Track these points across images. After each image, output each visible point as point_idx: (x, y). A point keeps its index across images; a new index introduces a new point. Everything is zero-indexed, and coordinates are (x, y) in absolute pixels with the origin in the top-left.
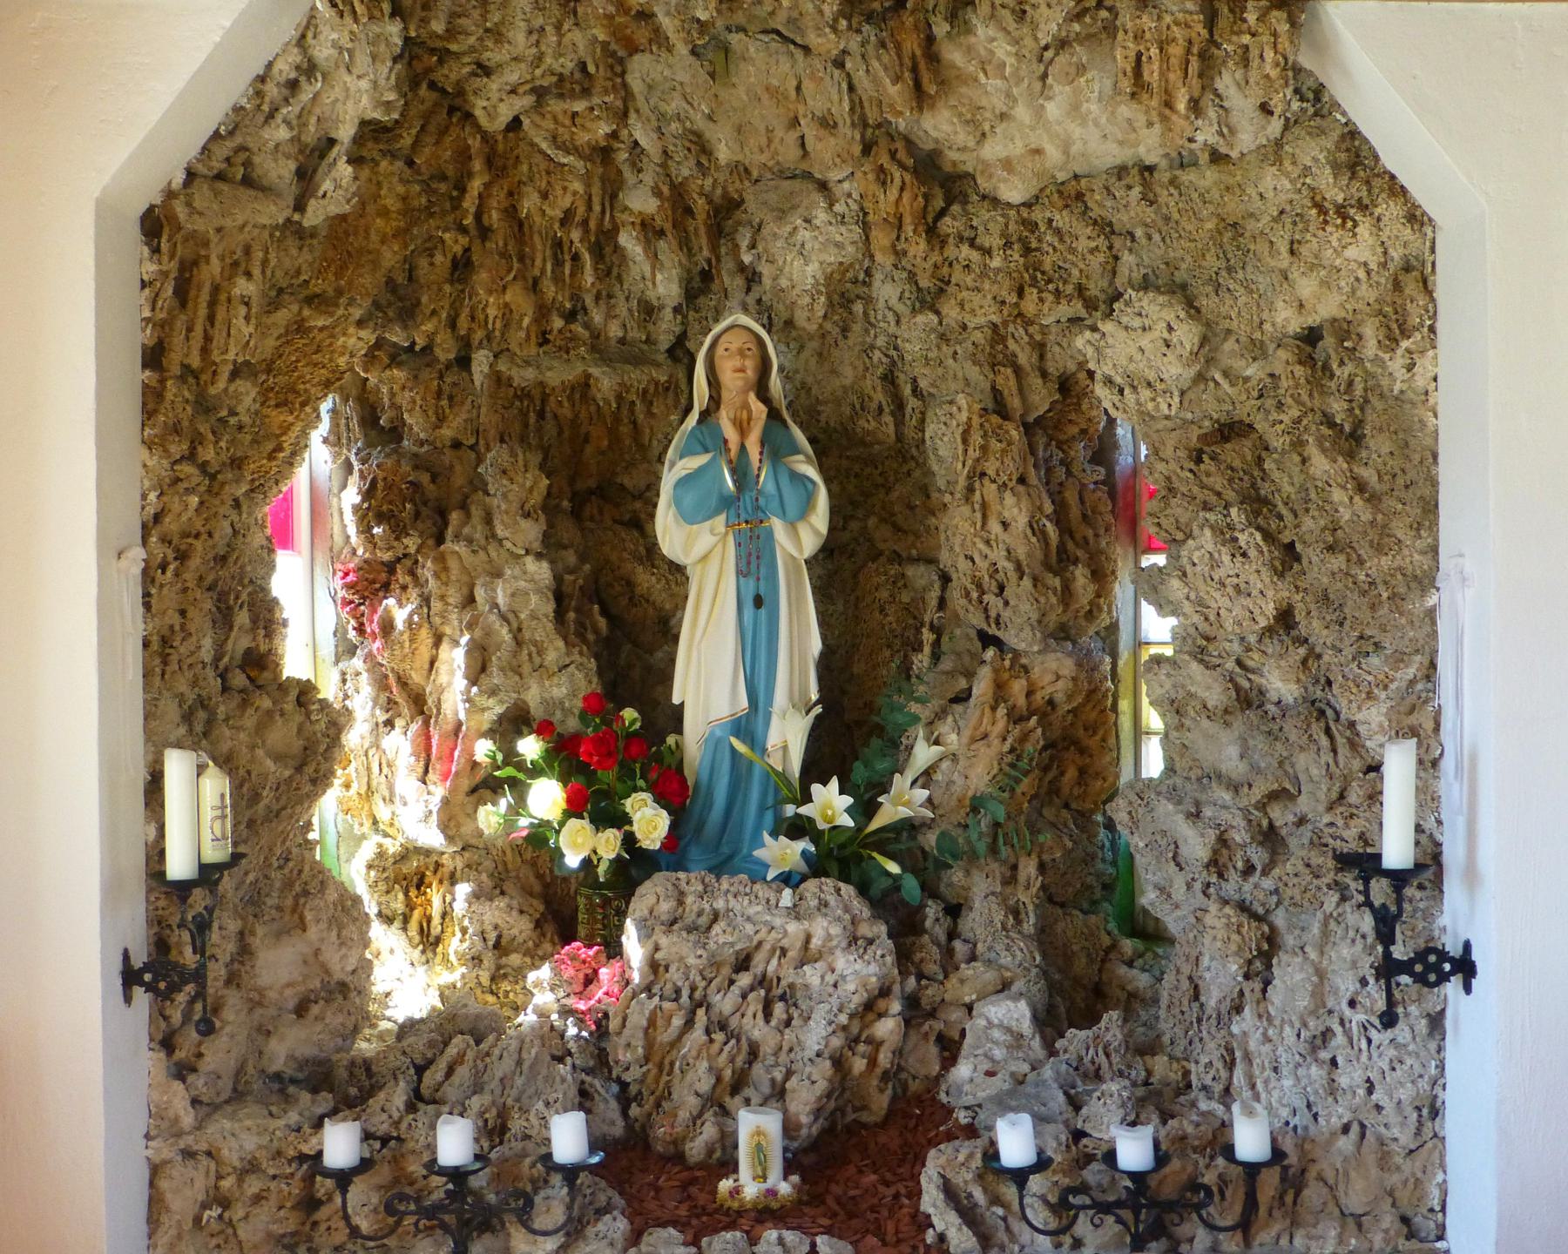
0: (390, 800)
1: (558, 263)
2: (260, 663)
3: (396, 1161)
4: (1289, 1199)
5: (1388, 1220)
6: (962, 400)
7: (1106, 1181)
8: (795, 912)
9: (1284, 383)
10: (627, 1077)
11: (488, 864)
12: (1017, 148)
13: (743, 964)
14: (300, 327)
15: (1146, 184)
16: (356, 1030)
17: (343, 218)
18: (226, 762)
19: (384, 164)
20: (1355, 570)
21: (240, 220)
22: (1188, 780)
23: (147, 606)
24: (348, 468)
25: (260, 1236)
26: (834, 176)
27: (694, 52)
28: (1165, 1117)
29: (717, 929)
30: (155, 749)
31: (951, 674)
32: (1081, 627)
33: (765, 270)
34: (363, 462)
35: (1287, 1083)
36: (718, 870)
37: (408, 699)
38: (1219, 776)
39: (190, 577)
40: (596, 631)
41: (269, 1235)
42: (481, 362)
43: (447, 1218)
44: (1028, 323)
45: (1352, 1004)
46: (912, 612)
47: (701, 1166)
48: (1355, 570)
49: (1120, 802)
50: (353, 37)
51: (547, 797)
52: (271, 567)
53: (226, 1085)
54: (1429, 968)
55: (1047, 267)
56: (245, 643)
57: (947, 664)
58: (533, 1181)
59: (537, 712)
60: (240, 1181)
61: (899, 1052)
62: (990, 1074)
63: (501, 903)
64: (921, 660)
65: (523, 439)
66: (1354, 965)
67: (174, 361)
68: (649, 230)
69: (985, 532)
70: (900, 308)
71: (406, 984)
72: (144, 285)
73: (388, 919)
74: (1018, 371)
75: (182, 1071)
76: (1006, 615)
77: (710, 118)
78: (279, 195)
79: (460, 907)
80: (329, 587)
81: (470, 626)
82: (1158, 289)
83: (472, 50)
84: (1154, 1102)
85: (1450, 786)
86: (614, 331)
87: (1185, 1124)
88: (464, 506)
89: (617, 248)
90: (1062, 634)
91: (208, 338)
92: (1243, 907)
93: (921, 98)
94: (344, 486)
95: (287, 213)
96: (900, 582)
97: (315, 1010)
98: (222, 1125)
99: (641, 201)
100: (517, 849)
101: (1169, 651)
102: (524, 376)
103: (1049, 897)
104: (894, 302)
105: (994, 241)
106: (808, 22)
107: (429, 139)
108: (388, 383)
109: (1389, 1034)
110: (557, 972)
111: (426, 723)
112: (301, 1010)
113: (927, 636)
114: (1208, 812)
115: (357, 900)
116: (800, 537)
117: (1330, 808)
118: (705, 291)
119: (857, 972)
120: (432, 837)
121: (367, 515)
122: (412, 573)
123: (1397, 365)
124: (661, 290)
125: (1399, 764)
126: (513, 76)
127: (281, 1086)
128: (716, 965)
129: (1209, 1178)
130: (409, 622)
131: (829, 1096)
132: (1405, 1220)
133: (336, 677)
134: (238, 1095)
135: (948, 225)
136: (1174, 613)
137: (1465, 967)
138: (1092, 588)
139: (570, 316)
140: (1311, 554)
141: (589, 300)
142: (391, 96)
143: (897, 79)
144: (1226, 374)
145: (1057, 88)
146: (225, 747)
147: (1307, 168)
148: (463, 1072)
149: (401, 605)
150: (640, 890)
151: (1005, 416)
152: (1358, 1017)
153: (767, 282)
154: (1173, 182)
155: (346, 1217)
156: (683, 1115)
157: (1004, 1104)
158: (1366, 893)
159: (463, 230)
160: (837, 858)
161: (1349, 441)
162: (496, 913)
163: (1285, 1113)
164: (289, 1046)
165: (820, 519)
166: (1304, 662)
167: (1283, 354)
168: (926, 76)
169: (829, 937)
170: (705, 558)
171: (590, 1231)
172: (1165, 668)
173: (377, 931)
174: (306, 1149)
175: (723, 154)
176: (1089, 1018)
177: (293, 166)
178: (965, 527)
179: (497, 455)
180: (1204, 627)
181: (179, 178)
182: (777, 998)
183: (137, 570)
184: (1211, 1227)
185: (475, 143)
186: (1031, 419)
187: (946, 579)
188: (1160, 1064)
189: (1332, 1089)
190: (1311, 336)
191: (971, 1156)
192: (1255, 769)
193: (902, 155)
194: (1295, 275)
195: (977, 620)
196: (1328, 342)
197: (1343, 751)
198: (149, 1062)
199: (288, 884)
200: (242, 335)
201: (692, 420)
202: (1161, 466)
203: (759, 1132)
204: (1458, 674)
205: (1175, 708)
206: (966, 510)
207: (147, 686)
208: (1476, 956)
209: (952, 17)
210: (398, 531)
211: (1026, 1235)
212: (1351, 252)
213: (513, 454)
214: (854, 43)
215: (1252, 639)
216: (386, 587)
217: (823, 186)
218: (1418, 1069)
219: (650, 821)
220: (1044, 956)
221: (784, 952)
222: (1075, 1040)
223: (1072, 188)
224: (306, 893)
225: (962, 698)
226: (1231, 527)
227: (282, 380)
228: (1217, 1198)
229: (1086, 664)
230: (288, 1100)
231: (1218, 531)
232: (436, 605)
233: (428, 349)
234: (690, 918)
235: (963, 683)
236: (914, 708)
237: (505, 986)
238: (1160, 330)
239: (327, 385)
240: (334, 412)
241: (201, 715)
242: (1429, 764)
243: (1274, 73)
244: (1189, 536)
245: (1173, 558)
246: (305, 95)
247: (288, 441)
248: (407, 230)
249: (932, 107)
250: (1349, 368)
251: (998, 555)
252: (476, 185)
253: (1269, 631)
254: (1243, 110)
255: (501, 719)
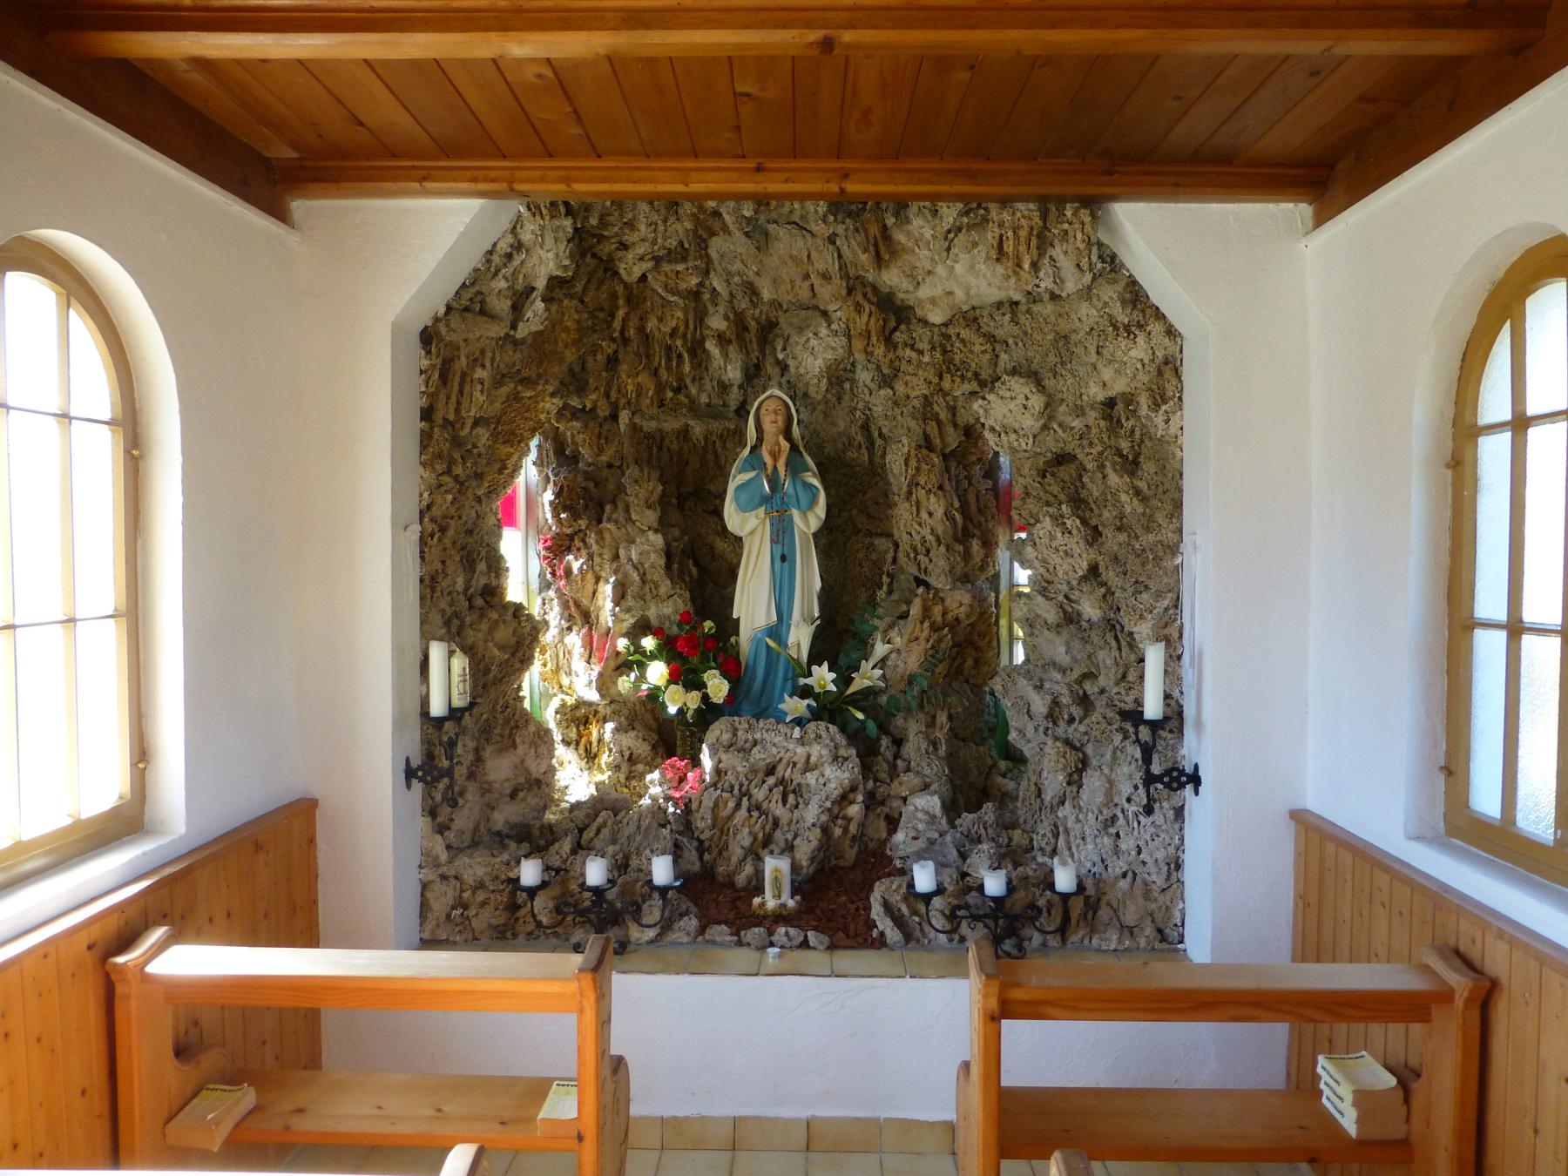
0: (569, 673)
1: (669, 359)
2: (492, 593)
3: (564, 883)
4: (1090, 915)
5: (1149, 930)
6: (905, 440)
7: (979, 902)
8: (802, 741)
9: (1094, 431)
10: (703, 837)
11: (625, 711)
12: (938, 292)
13: (771, 771)
14: (516, 397)
15: (1014, 313)
16: (545, 807)
17: (540, 333)
18: (469, 651)
19: (566, 302)
20: (1133, 542)
21: (478, 334)
22: (1037, 669)
23: (422, 558)
24: (547, 479)
25: (485, 925)
26: (831, 308)
27: (747, 234)
28: (1016, 865)
29: (755, 750)
30: (426, 637)
31: (898, 602)
32: (976, 574)
33: (791, 363)
34: (556, 475)
35: (1090, 847)
36: (758, 717)
37: (580, 614)
38: (1054, 664)
39: (447, 542)
40: (691, 576)
41: (490, 925)
42: (624, 417)
43: (592, 916)
44: (946, 394)
45: (1129, 800)
46: (878, 565)
47: (744, 889)
48: (1133, 542)
49: (997, 679)
50: (542, 228)
51: (657, 672)
52: (499, 536)
53: (467, 838)
54: (1172, 780)
55: (957, 361)
56: (483, 580)
57: (895, 596)
58: (643, 896)
59: (654, 622)
60: (474, 893)
61: (862, 825)
62: (915, 838)
63: (632, 734)
64: (882, 594)
65: (649, 462)
66: (1130, 777)
67: (438, 417)
68: (722, 340)
69: (919, 518)
70: (872, 386)
71: (576, 781)
72: (421, 372)
73: (566, 743)
74: (939, 423)
75: (441, 829)
76: (930, 567)
77: (757, 274)
78: (501, 320)
79: (608, 736)
80: (536, 548)
81: (616, 572)
82: (1020, 375)
83: (617, 234)
84: (1008, 857)
85: (1187, 670)
86: (704, 399)
87: (1029, 870)
88: (614, 502)
89: (705, 350)
90: (965, 579)
91: (459, 403)
92: (1067, 742)
93: (879, 262)
94: (545, 490)
95: (506, 330)
96: (871, 547)
97: (521, 795)
98: (464, 860)
99: (717, 322)
100: (643, 703)
101: (1027, 590)
102: (649, 426)
103: (954, 735)
104: (868, 382)
105: (924, 346)
106: (811, 217)
107: (592, 287)
108: (571, 430)
109: (1151, 819)
110: (663, 775)
111: (590, 629)
112: (513, 795)
113: (885, 579)
114: (1047, 685)
115: (548, 731)
116: (808, 521)
117: (1117, 684)
118: (757, 376)
119: (836, 777)
120: (593, 696)
121: (556, 508)
122: (583, 541)
123: (1159, 420)
124: (730, 375)
125: (1154, 657)
126: (641, 250)
127: (500, 839)
128: (754, 771)
129: (1041, 903)
130: (581, 569)
131: (819, 849)
132: (1160, 931)
133: (539, 601)
134: (475, 844)
135: (898, 337)
136: (1030, 567)
137: (1195, 780)
138: (982, 552)
139: (677, 391)
140: (1108, 533)
141: (688, 381)
142: (567, 262)
143: (865, 251)
144: (1060, 425)
145: (961, 256)
146: (470, 641)
147: (1106, 303)
148: (605, 832)
149: (576, 559)
150: (712, 727)
151: (931, 448)
152: (1132, 809)
153: (792, 370)
154: (1028, 311)
155: (534, 916)
156: (734, 860)
157: (921, 856)
158: (1136, 733)
159: (613, 340)
160: (828, 709)
161: (1131, 466)
162: (629, 740)
163: (1088, 865)
164: (504, 816)
165: (821, 510)
166: (1104, 596)
167: (1093, 414)
168: (883, 249)
169: (821, 756)
170: (752, 533)
171: (676, 926)
172: (1024, 600)
173: (561, 752)
174: (512, 875)
175: (766, 295)
176: (975, 807)
177: (509, 303)
178: (907, 515)
179: (632, 471)
180: (1046, 575)
181: (442, 310)
182: (791, 792)
183: (416, 537)
184: (1042, 931)
185: (620, 289)
186: (947, 451)
187: (896, 545)
188: (1017, 835)
189: (1116, 851)
190: (1110, 403)
191: (900, 886)
192: (1075, 660)
193: (870, 295)
194: (1099, 366)
195: (913, 570)
196: (1120, 406)
197: (1125, 649)
198: (421, 823)
199: (507, 722)
200: (478, 402)
201: (748, 449)
202: (1021, 480)
203: (776, 870)
204: (1193, 605)
205: (1029, 624)
206: (907, 505)
207: (422, 605)
208: (1201, 773)
209: (897, 214)
210: (575, 516)
211: (932, 934)
212: (1133, 353)
213: (642, 471)
214: (840, 229)
215: (1074, 583)
216: (569, 550)
217: (825, 314)
218: (1168, 840)
219: (717, 687)
220: (951, 770)
221: (795, 764)
222: (967, 819)
223: (971, 315)
224: (517, 727)
225: (904, 616)
226: (1062, 516)
227: (507, 428)
228: (1045, 914)
229: (979, 599)
230: (504, 847)
231: (1054, 518)
232: (597, 560)
233: (593, 410)
234: (740, 744)
235: (904, 608)
236: (877, 622)
237: (634, 783)
238: (1021, 399)
239: (533, 431)
240: (539, 447)
241: (456, 622)
242: (1173, 658)
243: (1082, 246)
244: (1038, 521)
245: (1030, 534)
246: (516, 262)
247: (510, 463)
248: (580, 340)
249: (887, 267)
250: (1132, 422)
251: (926, 532)
252: (621, 313)
253: (1084, 578)
254: (1066, 268)
255: (635, 626)
